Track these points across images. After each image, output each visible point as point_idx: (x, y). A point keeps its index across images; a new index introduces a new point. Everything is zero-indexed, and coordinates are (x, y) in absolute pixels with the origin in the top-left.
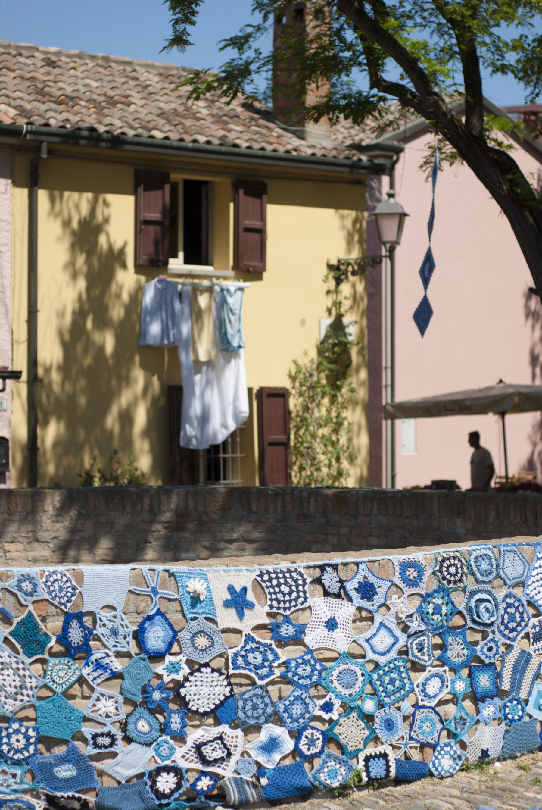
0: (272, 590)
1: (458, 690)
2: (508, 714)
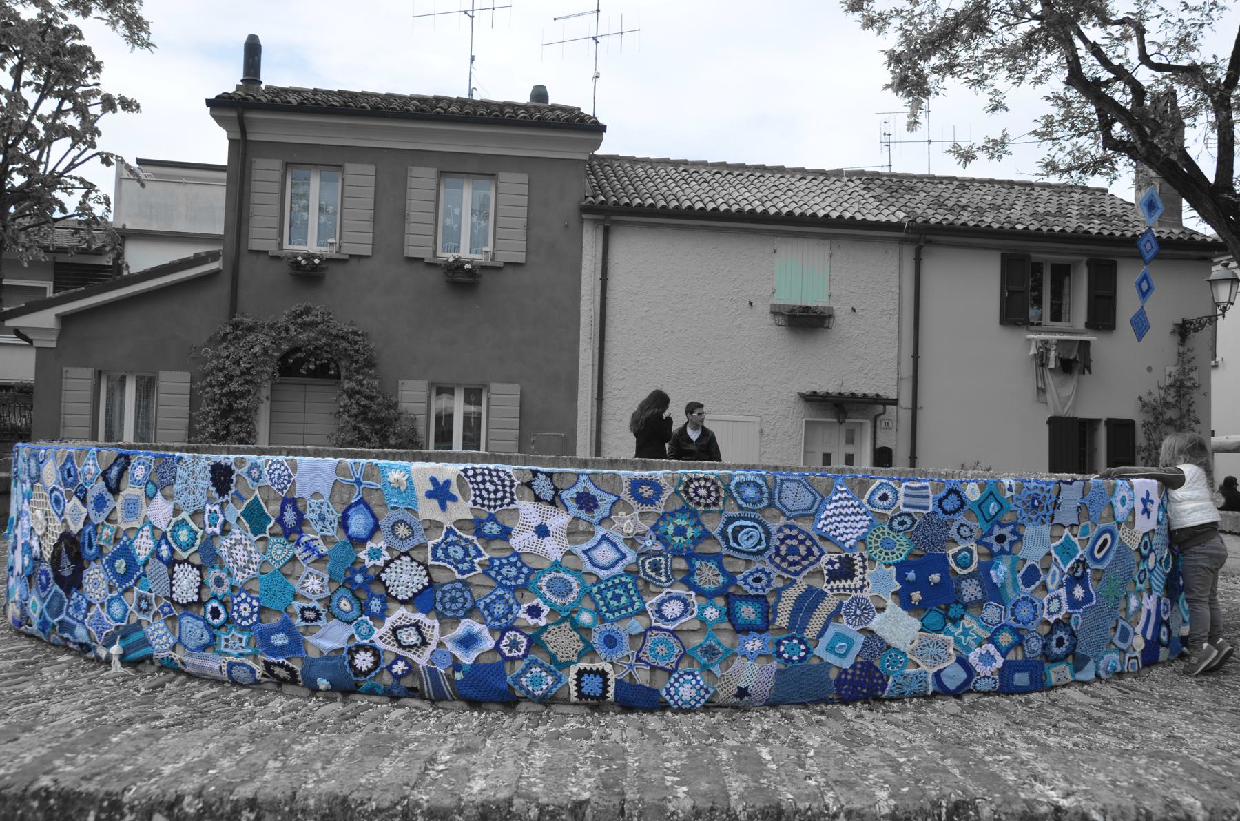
1: (708, 617)
2: (784, 652)
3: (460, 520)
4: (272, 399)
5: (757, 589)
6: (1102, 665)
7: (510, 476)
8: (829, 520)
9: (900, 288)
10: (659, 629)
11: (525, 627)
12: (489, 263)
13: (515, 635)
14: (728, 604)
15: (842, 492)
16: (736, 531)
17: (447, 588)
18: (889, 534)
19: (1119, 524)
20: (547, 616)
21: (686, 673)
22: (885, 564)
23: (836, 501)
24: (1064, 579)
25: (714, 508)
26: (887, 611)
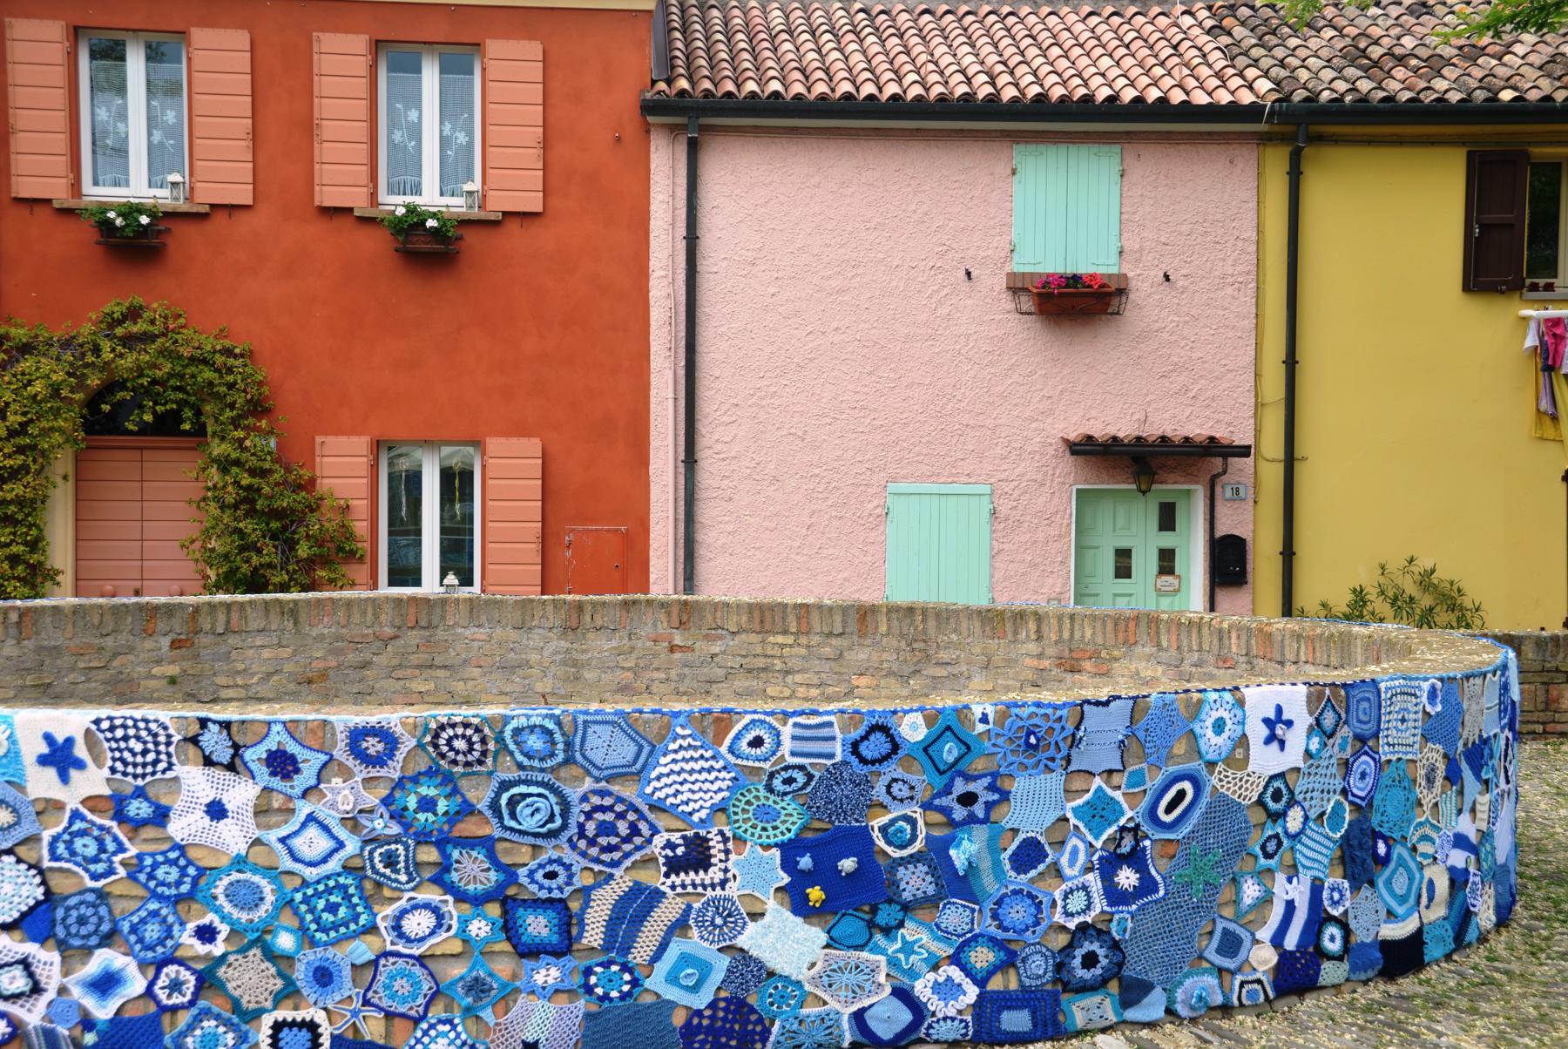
0: (114, 745)
1: (473, 934)
2: (596, 985)
3: (90, 798)
4: (80, 478)
5: (550, 890)
6: (1180, 994)
7: (166, 728)
8: (664, 780)
9: (1260, 230)
10: (398, 955)
11: (193, 958)
12: (476, 213)
13: (177, 972)
14: (505, 913)
15: (684, 737)
16: (513, 802)
17: (72, 901)
18: (767, 798)
19: (1211, 765)
20: (226, 940)
21: (440, 1021)
22: (761, 845)
23: (676, 752)
24: (1096, 857)
25: (479, 768)
26: (767, 918)
